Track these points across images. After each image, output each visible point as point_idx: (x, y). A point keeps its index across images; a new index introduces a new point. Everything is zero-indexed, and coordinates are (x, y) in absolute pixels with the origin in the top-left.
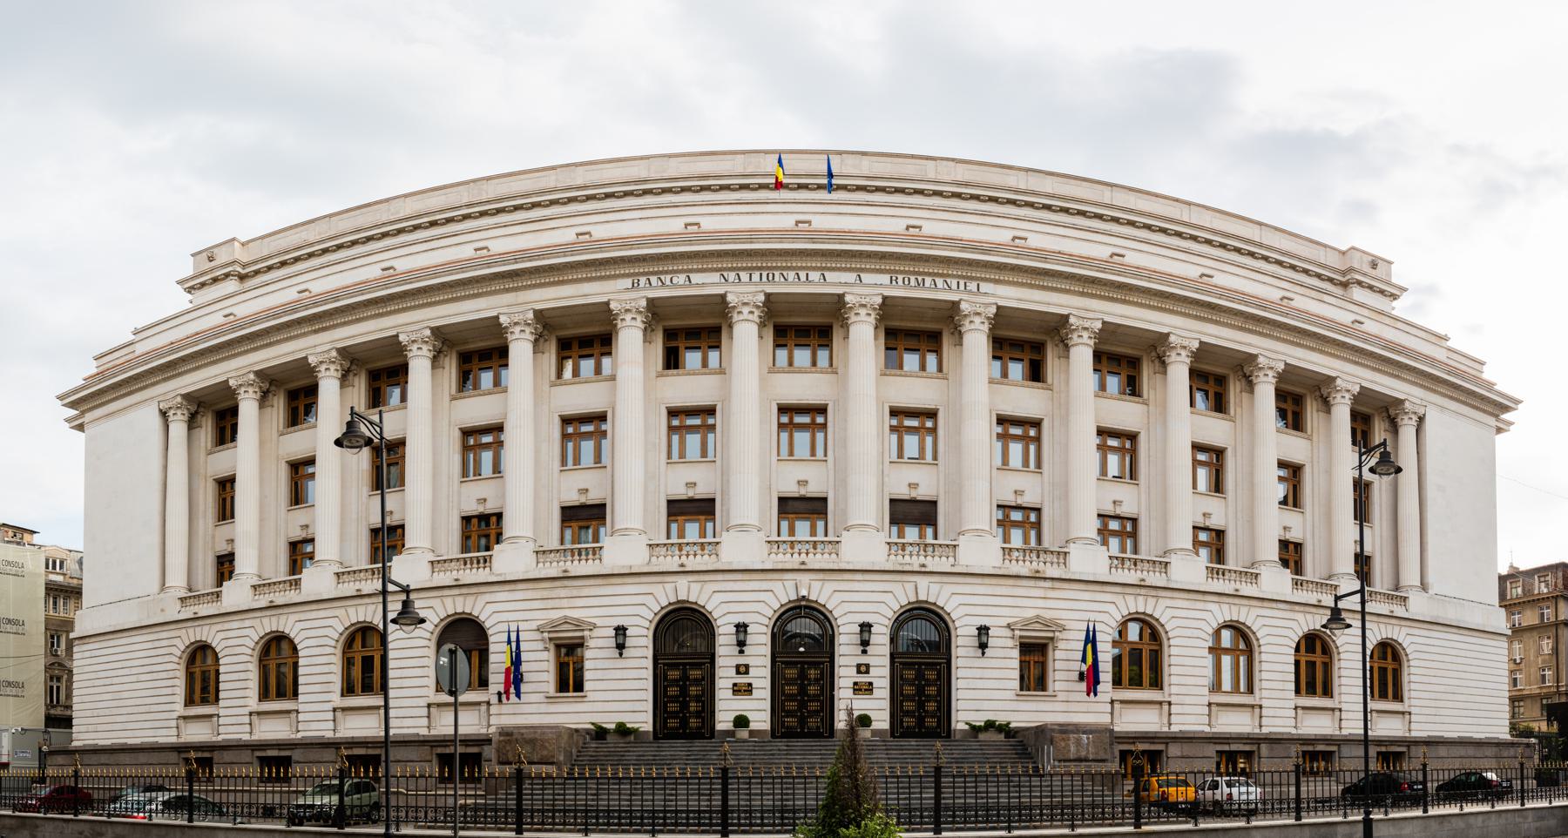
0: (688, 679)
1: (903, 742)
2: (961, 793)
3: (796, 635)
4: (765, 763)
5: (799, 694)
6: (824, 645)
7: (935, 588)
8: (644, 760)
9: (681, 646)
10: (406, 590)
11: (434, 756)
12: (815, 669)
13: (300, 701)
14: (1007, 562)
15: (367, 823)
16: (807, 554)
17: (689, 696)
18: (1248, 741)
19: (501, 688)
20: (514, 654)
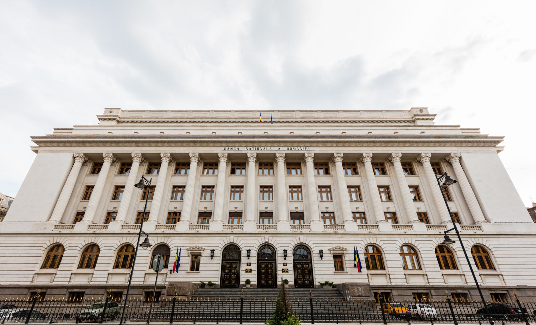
0: (232, 267)
1: (299, 289)
2: (319, 308)
3: (265, 254)
4: (255, 296)
5: (266, 273)
6: (273, 256)
7: (305, 239)
8: (216, 295)
9: (231, 256)
10: (147, 235)
11: (144, 293)
12: (270, 264)
13: (95, 270)
14: (326, 229)
15: (109, 320)
16: (268, 229)
17: (232, 273)
18: (425, 289)
19: (172, 269)
20: (178, 257)
